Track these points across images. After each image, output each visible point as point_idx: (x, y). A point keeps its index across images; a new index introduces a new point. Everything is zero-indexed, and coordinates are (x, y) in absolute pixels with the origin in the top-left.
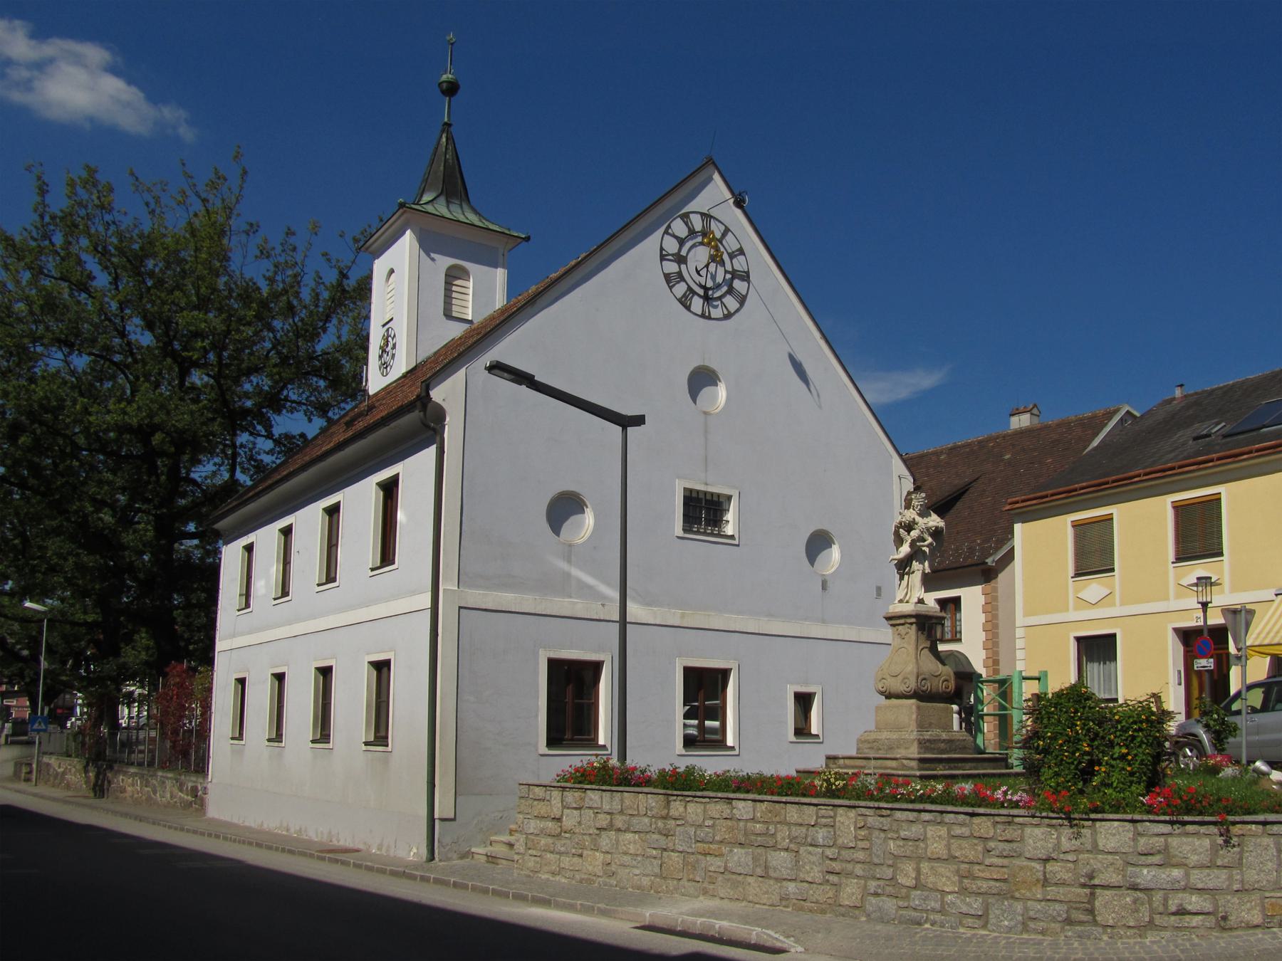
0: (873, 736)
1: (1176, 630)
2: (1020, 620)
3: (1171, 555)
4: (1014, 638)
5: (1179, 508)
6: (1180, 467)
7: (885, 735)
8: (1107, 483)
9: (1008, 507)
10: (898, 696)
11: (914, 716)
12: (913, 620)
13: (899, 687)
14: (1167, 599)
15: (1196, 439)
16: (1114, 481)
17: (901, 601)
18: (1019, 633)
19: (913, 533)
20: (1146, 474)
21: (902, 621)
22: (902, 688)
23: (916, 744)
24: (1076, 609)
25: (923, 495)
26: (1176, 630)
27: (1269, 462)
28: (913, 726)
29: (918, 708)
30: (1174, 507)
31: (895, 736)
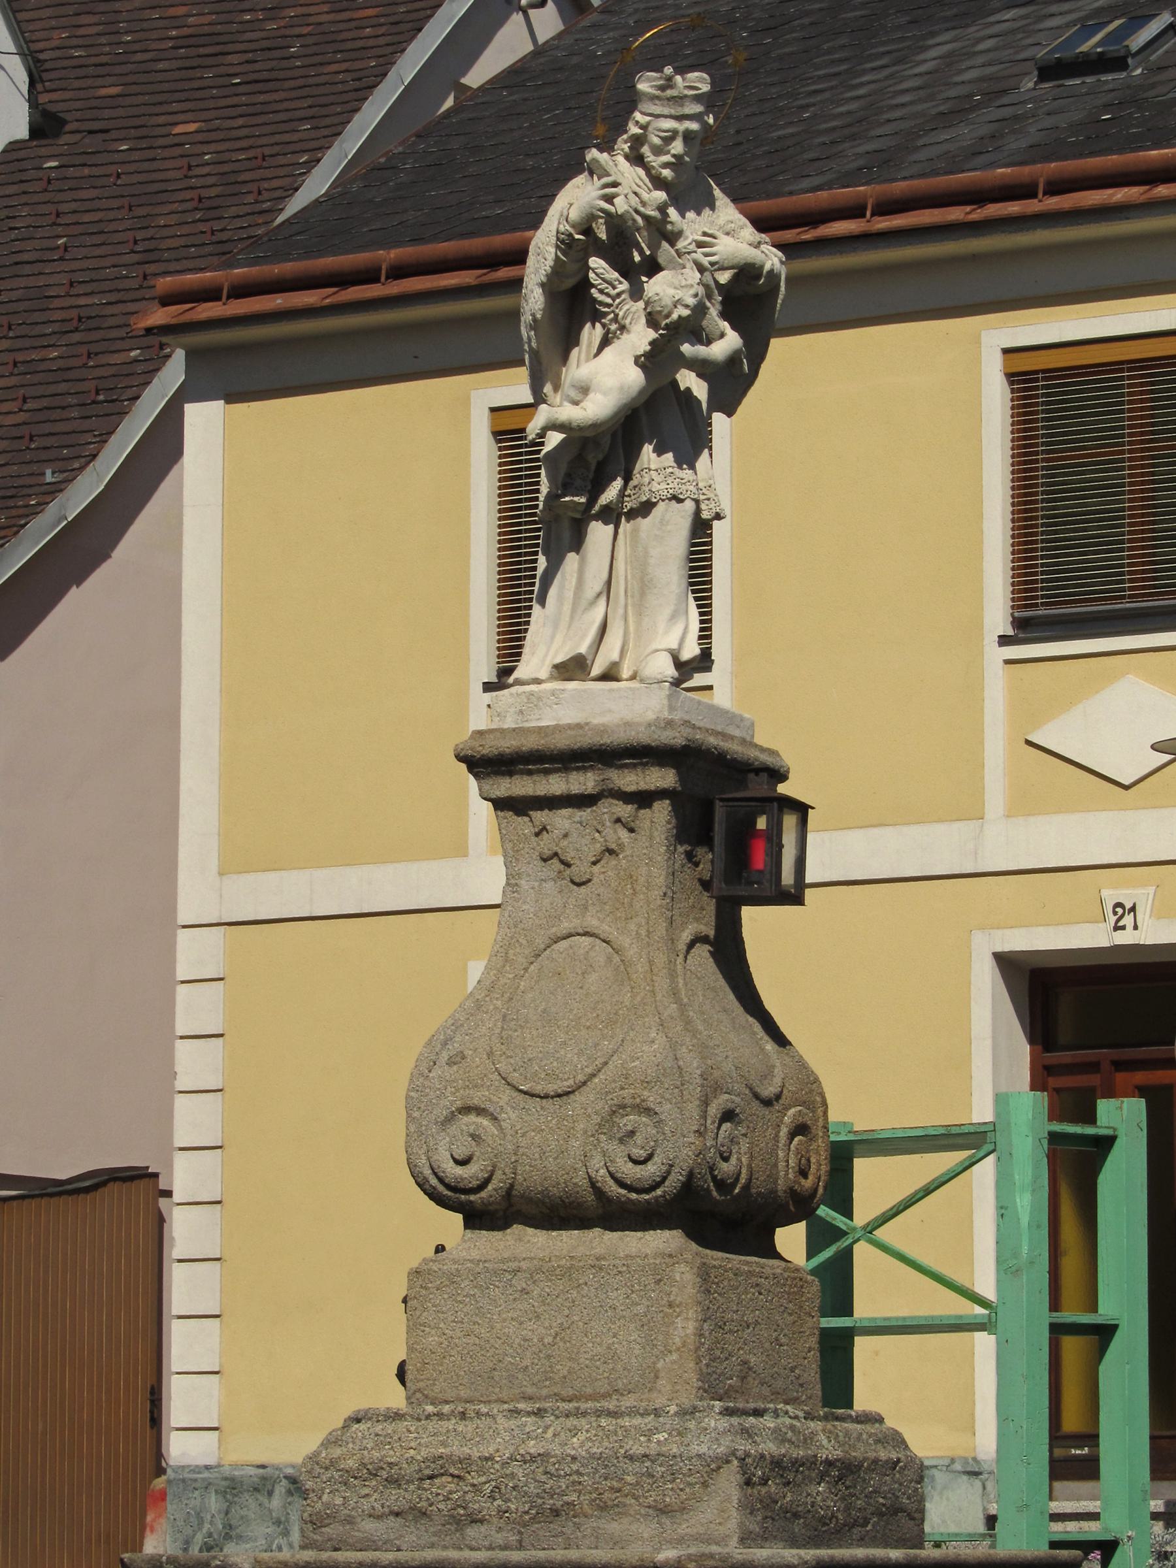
0: (420, 1443)
1: (1007, 963)
2: (199, 891)
3: (997, 615)
4: (168, 983)
5: (1038, 386)
6: (1057, 187)
7: (499, 1437)
8: (369, 276)
9: (159, 316)
10: (557, 1213)
11: (685, 1327)
12: (662, 778)
13: (563, 1149)
14: (971, 811)
15: (1050, 71)
16: (399, 272)
17: (573, 668)
18: (194, 953)
19: (659, 287)
20: (887, 208)
21: (583, 782)
22: (605, 1163)
23: (729, 1483)
24: (1023, 803)
25: (700, 81)
26: (1007, 963)
27: (975, 258)
28: (677, 1382)
29: (704, 1273)
30: (1012, 377)
31: (580, 1440)
